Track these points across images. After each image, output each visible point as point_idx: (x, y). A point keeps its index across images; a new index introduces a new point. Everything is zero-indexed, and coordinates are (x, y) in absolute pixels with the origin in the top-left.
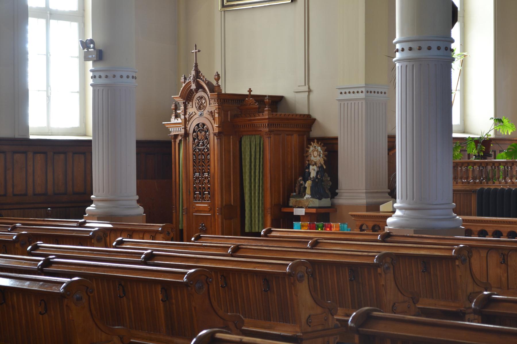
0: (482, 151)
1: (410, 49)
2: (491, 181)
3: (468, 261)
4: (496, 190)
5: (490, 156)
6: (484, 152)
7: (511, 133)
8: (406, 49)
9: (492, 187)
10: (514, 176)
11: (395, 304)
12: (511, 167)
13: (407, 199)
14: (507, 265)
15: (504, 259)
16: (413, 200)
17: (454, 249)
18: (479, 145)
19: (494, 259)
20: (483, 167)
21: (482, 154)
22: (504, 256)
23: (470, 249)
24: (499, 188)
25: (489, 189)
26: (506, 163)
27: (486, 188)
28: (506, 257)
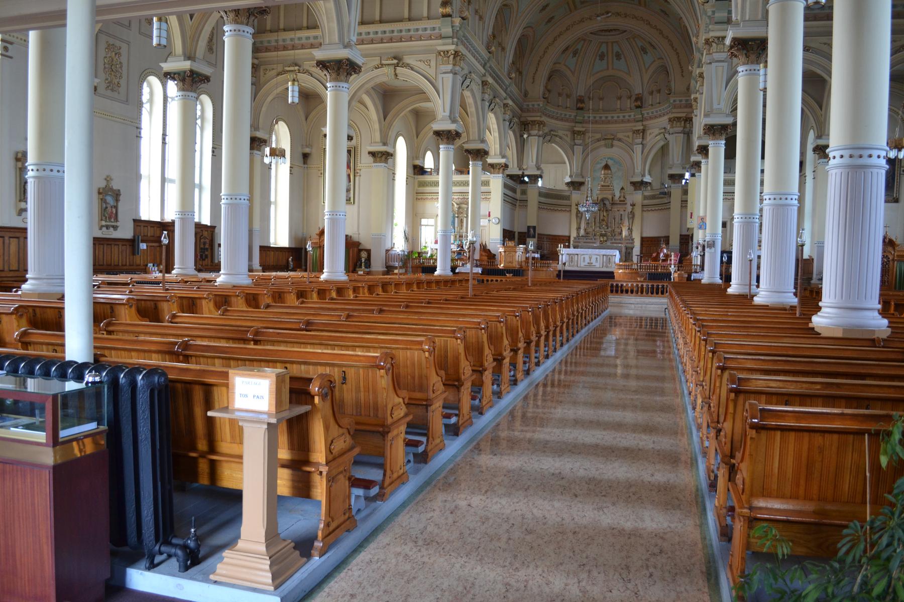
1: (38, 170)
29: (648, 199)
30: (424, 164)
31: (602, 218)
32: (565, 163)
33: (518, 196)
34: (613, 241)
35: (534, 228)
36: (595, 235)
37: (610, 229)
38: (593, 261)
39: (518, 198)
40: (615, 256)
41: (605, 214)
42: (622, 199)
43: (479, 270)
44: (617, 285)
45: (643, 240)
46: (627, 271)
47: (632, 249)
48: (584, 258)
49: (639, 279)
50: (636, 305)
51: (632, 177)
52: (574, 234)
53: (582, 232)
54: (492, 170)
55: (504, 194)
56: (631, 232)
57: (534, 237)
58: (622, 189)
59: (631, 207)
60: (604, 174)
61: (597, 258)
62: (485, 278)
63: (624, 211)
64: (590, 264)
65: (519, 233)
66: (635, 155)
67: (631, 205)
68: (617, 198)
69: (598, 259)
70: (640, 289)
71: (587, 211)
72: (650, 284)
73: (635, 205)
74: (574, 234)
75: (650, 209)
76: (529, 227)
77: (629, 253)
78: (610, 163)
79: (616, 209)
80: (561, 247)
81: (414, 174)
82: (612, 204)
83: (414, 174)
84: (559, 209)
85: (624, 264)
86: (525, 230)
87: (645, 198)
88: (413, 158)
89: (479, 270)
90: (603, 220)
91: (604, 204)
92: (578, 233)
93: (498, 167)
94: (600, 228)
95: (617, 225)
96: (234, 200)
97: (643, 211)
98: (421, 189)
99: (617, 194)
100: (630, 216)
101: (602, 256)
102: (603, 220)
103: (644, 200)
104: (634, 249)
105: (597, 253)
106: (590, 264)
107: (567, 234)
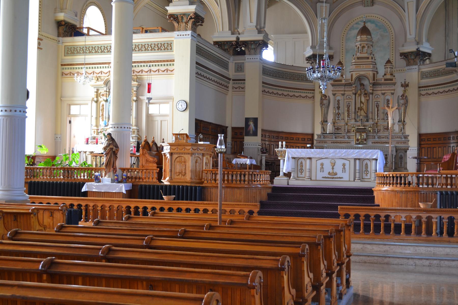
0: (31, 162)
1: (6, 111)
2: (36, 177)
3: (37, 215)
4: (38, 182)
5: (35, 164)
6: (32, 162)
7: (46, 153)
8: (113, 127)
9: (37, 181)
10: (45, 175)
11: (3, 235)
12: (46, 170)
13: (1, 185)
14: (53, 217)
15: (51, 214)
16: (5, 186)
17: (30, 209)
18: (30, 159)
19: (47, 214)
20: (31, 170)
21: (31, 163)
22: (52, 213)
23: (38, 210)
24: (40, 181)
25: (35, 182)
26: (44, 168)
27: (33, 181)
28: (52, 213)
29: (427, 77)
30: (81, 20)
31: (358, 105)
32: (306, 32)
33: (231, 73)
34: (377, 140)
35: (255, 120)
36: (349, 131)
37: (371, 122)
38: (338, 169)
39: (231, 77)
40: (376, 160)
41: (363, 99)
42: (388, 76)
43: (123, 188)
44: (377, 217)
45: (422, 138)
46: (398, 188)
47: (406, 151)
48: (322, 165)
49: (422, 205)
50: (417, 262)
51: (403, 46)
52: (318, 131)
53: (329, 128)
54: (176, 24)
55: (197, 63)
56: (404, 125)
57: (255, 134)
58: (389, 62)
59: (403, 89)
60: (361, 41)
61: (344, 165)
62: (133, 203)
63: (393, 94)
64: (333, 175)
65: (233, 128)
66: (406, 14)
67: (402, 86)
68: (380, 76)
69: (347, 167)
70: (424, 226)
71: (321, 78)
72: (445, 216)
73: (407, 85)
74: (318, 131)
75: (431, 91)
76: (247, 120)
77: (401, 158)
78: (369, 26)
79: (379, 92)
80: (282, 145)
81: (59, 36)
82: (374, 84)
83: (59, 36)
84: (291, 94)
85: (395, 174)
86: (242, 124)
87: (424, 75)
88: (55, 9)
89: (123, 188)
90: (360, 109)
91: (362, 85)
92: (324, 129)
93: (185, 20)
94: (356, 121)
95: (381, 116)
96: (119, 128)
97: (420, 95)
98: (69, 59)
99: (381, 71)
100: (402, 102)
101: (352, 162)
102: (360, 109)
103: (422, 78)
104: (408, 152)
105: (343, 156)
106: (333, 175)
107: (309, 131)
